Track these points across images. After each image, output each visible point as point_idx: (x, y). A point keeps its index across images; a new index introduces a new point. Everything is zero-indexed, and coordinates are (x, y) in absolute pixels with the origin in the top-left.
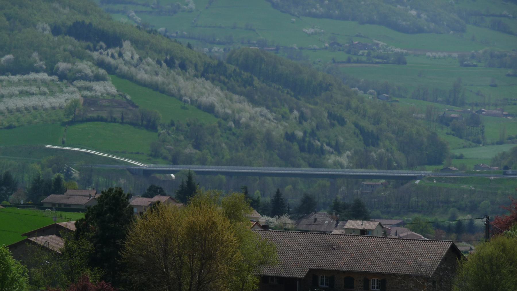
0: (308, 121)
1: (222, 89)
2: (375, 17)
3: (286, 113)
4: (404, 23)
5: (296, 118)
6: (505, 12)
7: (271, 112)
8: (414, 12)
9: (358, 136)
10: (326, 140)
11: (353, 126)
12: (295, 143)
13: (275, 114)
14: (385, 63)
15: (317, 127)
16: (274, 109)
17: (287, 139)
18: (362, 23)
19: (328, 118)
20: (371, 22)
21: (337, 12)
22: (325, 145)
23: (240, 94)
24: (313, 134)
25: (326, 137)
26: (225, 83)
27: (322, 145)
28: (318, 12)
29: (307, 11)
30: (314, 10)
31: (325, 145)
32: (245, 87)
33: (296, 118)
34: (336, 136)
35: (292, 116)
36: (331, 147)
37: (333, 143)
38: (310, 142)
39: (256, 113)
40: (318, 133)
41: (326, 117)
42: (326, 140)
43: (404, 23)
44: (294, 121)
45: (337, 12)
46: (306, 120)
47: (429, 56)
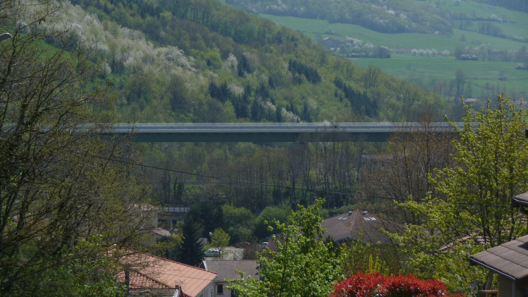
0: (255, 73)
1: (100, 18)
2: (347, 15)
3: (215, 59)
4: (381, 21)
5: (233, 66)
6: (493, 16)
7: (187, 54)
8: (391, 12)
9: (341, 100)
10: (285, 103)
11: (333, 86)
12: (228, 103)
13: (195, 60)
14: (363, 56)
15: (271, 82)
16: (193, 51)
17: (213, 95)
18: (333, 21)
19: (289, 69)
20: (343, 20)
21: (302, 9)
22: (284, 110)
23: (137, 27)
24: (263, 92)
25: (286, 98)
26: (106, 11)
27: (279, 109)
28: (280, 8)
29: (267, 7)
30: (276, 7)
31: (284, 110)
32: (143, 17)
33: (233, 66)
34: (303, 98)
35: (226, 65)
36: (295, 112)
37: (300, 108)
38: (255, 102)
39: (158, 55)
40: (271, 92)
41: (286, 69)
42: (285, 103)
43: (381, 21)
44: (229, 71)
45: (302, 9)
46: (249, 71)
47: (415, 53)
